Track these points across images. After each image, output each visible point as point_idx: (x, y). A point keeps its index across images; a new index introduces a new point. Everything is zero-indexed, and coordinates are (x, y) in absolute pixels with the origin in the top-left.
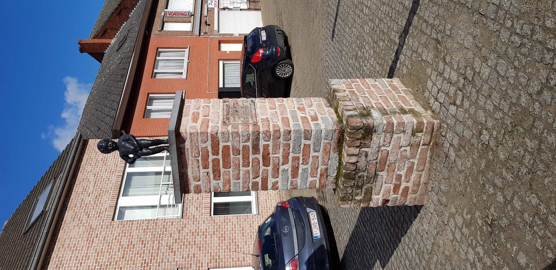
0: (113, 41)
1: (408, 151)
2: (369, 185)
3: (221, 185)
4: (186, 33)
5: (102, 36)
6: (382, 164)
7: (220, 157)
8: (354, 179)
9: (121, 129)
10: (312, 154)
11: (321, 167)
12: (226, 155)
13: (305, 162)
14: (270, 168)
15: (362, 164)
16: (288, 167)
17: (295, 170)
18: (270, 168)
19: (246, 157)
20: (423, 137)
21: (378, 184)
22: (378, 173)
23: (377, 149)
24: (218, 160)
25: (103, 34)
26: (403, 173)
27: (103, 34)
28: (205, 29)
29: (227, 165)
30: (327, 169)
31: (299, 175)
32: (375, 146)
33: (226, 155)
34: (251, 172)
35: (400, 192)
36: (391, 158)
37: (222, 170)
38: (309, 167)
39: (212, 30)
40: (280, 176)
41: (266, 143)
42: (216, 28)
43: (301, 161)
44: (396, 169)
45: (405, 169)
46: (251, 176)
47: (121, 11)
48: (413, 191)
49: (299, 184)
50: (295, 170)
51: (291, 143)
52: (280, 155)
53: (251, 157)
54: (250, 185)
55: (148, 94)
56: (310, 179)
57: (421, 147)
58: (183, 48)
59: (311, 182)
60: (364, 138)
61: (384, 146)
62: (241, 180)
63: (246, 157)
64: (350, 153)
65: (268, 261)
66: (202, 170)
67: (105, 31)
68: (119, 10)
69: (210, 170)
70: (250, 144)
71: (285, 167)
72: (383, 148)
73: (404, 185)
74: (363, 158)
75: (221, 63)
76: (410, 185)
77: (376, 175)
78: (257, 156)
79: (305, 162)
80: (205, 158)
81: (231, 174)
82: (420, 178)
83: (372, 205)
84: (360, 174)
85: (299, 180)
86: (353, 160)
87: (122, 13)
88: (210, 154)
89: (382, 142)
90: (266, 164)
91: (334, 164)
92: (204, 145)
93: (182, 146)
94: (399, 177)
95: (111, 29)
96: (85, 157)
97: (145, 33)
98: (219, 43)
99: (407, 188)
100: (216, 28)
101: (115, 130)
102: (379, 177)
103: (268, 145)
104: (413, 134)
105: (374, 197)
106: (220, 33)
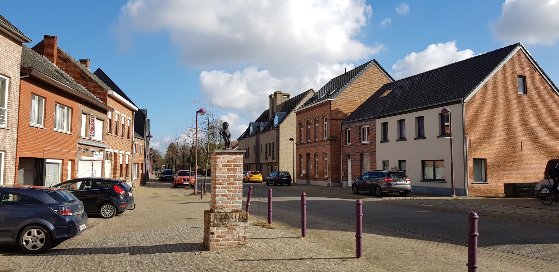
0: (55, 65)
4: (80, 133)
5: (60, 57)
6: (231, 228)
7: (232, 167)
9: (30, 75)
10: (232, 201)
11: (226, 206)
14: (226, 185)
15: (231, 220)
16: (227, 192)
17: (225, 195)
18: (226, 185)
19: (232, 176)
20: (242, 242)
25: (62, 59)
26: (227, 237)
27: (62, 59)
28: (83, 147)
36: (234, 231)
39: (81, 155)
42: (84, 158)
47: (85, 78)
50: (225, 195)
51: (237, 193)
53: (232, 178)
55: (45, 98)
56: (220, 202)
58: (71, 130)
63: (232, 176)
65: (11, 198)
67: (64, 60)
68: (86, 77)
69: (227, 163)
70: (237, 178)
71: (227, 191)
73: (221, 239)
75: (60, 161)
76: (221, 242)
77: (226, 227)
80: (232, 162)
83: (211, 228)
86: (234, 216)
87: (83, 79)
90: (228, 184)
91: (227, 210)
94: (225, 236)
95: (67, 67)
96: (11, 42)
97: (83, 99)
98: (72, 160)
100: (84, 158)
101: (32, 70)
104: (244, 237)
106: (80, 162)
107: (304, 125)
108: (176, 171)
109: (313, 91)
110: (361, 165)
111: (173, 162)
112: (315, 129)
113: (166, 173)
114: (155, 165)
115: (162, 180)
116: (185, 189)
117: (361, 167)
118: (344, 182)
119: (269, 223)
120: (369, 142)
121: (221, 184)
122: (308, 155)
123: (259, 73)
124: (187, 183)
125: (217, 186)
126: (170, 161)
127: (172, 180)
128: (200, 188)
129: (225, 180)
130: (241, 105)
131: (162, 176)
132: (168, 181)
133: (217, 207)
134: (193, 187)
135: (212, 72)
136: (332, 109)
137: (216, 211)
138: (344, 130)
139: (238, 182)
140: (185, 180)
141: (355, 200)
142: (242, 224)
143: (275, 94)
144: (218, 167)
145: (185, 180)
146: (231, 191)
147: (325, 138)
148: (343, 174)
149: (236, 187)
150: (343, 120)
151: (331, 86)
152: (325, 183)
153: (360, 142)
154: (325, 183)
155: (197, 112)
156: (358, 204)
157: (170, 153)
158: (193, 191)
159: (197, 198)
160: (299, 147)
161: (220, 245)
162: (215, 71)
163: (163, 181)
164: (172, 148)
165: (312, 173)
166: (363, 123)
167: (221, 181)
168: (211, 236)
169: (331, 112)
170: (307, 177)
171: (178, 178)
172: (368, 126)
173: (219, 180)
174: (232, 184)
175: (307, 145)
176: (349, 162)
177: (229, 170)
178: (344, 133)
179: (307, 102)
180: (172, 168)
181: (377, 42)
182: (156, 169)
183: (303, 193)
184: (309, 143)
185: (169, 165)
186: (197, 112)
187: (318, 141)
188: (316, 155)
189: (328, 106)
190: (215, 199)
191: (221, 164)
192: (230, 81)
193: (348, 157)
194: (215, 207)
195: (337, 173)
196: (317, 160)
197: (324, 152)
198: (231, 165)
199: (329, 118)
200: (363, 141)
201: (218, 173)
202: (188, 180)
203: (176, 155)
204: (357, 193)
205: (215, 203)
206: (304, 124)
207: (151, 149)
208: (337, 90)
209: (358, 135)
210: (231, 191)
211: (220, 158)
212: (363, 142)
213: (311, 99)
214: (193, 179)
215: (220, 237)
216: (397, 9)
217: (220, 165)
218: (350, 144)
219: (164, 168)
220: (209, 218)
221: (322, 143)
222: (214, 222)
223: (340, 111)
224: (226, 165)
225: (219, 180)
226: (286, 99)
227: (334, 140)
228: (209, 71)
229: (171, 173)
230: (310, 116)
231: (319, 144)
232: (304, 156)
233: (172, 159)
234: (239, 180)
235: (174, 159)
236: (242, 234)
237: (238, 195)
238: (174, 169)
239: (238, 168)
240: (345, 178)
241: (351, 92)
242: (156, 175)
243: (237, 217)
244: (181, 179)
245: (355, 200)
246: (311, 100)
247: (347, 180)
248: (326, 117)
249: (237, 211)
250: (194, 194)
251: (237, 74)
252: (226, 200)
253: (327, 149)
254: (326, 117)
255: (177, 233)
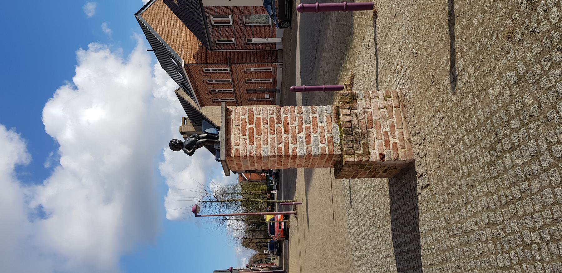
1: (386, 112)
2: (364, 140)
3: (254, 149)
6: (370, 124)
7: (254, 126)
8: (352, 135)
10: (319, 124)
12: (258, 125)
13: (315, 131)
14: (290, 136)
15: (355, 122)
16: (303, 134)
17: (308, 137)
18: (290, 136)
19: (272, 127)
20: (393, 102)
21: (372, 139)
22: (369, 130)
23: (363, 110)
24: (253, 128)
26: (388, 129)
29: (259, 134)
30: (332, 137)
31: (312, 142)
32: (361, 108)
33: (258, 125)
34: (276, 138)
35: (391, 147)
36: (375, 118)
37: (255, 136)
38: (318, 135)
40: (298, 142)
41: (285, 115)
43: (312, 131)
44: (382, 127)
45: (389, 127)
46: (276, 142)
48: (401, 146)
49: (312, 150)
50: (308, 137)
51: (303, 115)
52: (296, 125)
54: (276, 150)
56: (321, 146)
57: (394, 109)
59: (322, 148)
60: (351, 102)
61: (367, 108)
62: (269, 146)
63: (272, 127)
64: (344, 113)
66: (242, 137)
70: (274, 116)
71: (301, 135)
72: (367, 110)
73: (392, 141)
74: (355, 117)
76: (397, 140)
77: (368, 132)
78: (279, 125)
79: (315, 131)
81: (262, 140)
82: (403, 134)
83: (372, 159)
84: (355, 131)
85: (312, 146)
86: (348, 118)
88: (247, 123)
89: (365, 105)
90: (287, 132)
91: (336, 131)
92: (244, 117)
93: (229, 117)
94: (386, 134)
99: (395, 144)
102: (371, 133)
103: (287, 118)
105: (371, 151)
107: (215, 97)
108: (270, 238)
109: (178, 90)
110: (257, 26)
111: (260, 242)
112: (219, 84)
113: (272, 249)
114: (265, 261)
115: (279, 253)
116: (289, 226)
117: (260, 26)
118: (278, 47)
119: (341, 89)
120: (230, 16)
121: (287, 146)
122: (248, 91)
123: (166, 159)
124: (283, 224)
125: (291, 153)
126: (259, 246)
127: (279, 242)
128: (288, 207)
129: (280, 138)
130: (200, 176)
131: (275, 253)
132: (281, 246)
133: (331, 151)
134: (287, 217)
135: (166, 209)
136: (195, 62)
137: (338, 152)
138: (218, 47)
139: (283, 115)
140: (280, 227)
141: (298, 14)
142: (361, 103)
143: (182, 133)
144: (255, 153)
145: (280, 227)
146: (300, 126)
147: (229, 71)
148: (268, 49)
149: (293, 119)
150: (207, 49)
151: (169, 68)
152: (279, 70)
153: (231, 26)
154: (279, 70)
155: (196, 216)
156: (302, 9)
157: (251, 245)
158: (292, 217)
159: (301, 209)
160: (239, 102)
161: (404, 141)
162: (166, 205)
163: (281, 252)
164: (246, 244)
165: (268, 87)
166: (209, 23)
167: (282, 145)
168: (386, 159)
169: (198, 64)
170: (272, 93)
171: (277, 235)
172: (211, 16)
173: (280, 149)
174: (286, 126)
175: (238, 93)
176: (254, 40)
177: (261, 130)
178: (221, 47)
179: (189, 95)
180: (267, 243)
181: (131, 37)
182: (269, 259)
183: (292, 90)
184: (235, 90)
185: (264, 246)
186: (196, 216)
187: (233, 79)
188: (248, 82)
189: (191, 67)
190: (315, 156)
191: (249, 147)
192: (176, 190)
193: (249, 42)
194: (331, 156)
195: (268, 55)
196: (254, 99)
197: (245, 72)
198: (251, 129)
199: (205, 65)
200: (229, 23)
201: (266, 151)
202: (280, 223)
203: (252, 239)
204: (290, 21)
205: (323, 156)
206: (214, 97)
207: (247, 266)
208: (172, 57)
209: (223, 29)
210: (300, 126)
211: (237, 150)
212: (231, 24)
213: (185, 90)
214: (279, 216)
215: (387, 142)
216: (90, 15)
217: (251, 149)
218: (233, 40)
219: (267, 252)
220: (354, 164)
221: (235, 74)
222: (361, 155)
223: (196, 54)
224: (251, 137)
225: (280, 149)
226: (188, 122)
227: (230, 60)
228: (165, 212)
229: (272, 243)
230: (204, 96)
231: (235, 79)
232: (249, 96)
233: (257, 243)
234: (279, 112)
235: (258, 241)
236: (380, 103)
237: (307, 113)
238: (269, 241)
239: (255, 116)
240: (273, 46)
241: (174, 41)
242: (274, 259)
243: (348, 112)
244: (278, 231)
245: (298, 14)
246: (186, 89)
247: (274, 44)
248: (207, 80)
249: (337, 114)
250: (296, 215)
251: (170, 183)
252: (318, 135)
253: (241, 68)
254: (207, 80)
255: (363, 228)
